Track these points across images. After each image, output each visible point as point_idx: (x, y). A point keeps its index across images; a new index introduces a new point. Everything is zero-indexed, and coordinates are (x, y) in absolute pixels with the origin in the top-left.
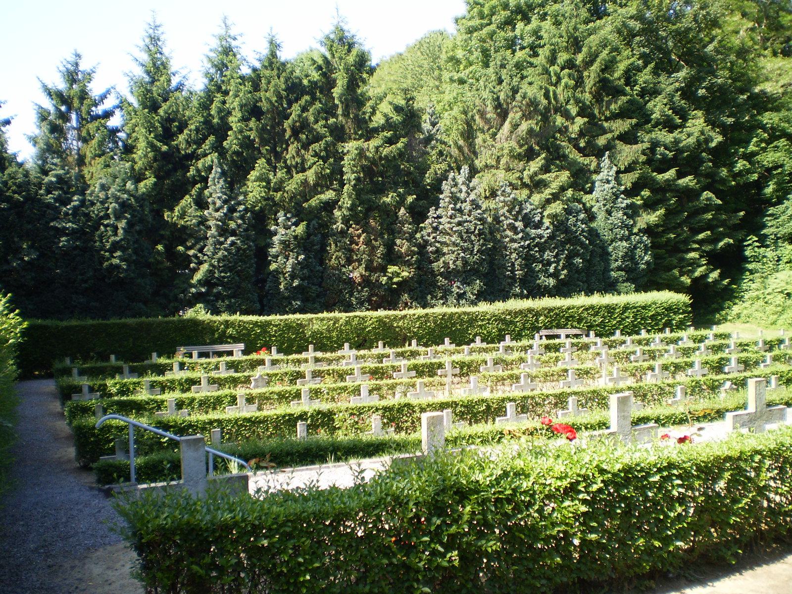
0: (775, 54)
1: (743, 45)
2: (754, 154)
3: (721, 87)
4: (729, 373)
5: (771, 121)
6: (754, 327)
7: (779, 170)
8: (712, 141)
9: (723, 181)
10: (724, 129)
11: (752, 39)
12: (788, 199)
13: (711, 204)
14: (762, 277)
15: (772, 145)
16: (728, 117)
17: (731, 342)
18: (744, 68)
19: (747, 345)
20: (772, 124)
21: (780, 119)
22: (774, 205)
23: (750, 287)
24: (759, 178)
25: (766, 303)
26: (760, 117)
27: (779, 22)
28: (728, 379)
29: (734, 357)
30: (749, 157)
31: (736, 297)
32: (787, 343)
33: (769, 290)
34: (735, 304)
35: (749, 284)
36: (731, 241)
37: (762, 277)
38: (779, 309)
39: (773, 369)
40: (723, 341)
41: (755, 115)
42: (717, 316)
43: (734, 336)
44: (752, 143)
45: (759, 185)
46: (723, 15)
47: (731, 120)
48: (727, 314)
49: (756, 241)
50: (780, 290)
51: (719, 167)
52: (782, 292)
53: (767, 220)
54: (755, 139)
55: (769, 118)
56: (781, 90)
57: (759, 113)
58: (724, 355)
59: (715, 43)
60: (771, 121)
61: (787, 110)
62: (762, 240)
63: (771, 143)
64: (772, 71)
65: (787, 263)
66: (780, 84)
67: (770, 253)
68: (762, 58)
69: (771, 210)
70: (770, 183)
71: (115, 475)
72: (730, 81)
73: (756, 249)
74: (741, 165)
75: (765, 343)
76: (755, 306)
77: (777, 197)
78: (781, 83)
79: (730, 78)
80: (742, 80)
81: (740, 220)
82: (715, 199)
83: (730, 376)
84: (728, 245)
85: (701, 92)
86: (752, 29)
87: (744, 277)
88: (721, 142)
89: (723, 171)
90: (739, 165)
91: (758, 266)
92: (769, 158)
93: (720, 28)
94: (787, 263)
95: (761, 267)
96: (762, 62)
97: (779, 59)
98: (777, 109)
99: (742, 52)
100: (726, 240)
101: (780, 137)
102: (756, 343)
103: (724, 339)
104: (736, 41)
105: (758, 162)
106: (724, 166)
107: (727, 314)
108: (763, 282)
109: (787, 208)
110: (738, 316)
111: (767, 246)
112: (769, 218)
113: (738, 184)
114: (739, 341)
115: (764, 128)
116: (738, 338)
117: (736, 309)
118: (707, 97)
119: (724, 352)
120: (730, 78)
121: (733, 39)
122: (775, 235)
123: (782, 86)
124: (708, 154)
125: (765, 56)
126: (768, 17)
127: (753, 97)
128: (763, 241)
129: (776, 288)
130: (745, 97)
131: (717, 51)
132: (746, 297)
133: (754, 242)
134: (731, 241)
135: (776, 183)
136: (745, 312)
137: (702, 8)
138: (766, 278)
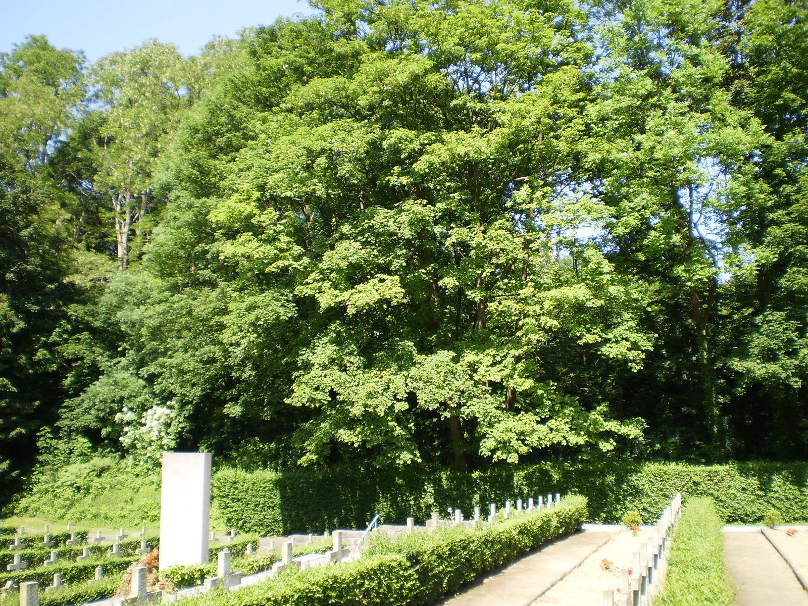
0: (88, 248)
1: (58, 235)
2: (56, 344)
3: (30, 273)
4: (11, 571)
5: (75, 314)
6: (41, 521)
7: (79, 363)
8: (14, 326)
9: (21, 368)
10: (28, 316)
11: (68, 230)
12: (85, 392)
13: (5, 392)
14: (52, 469)
15: (74, 337)
16: (33, 304)
17: (16, 538)
18: (55, 257)
19: (32, 541)
20: (77, 317)
21: (85, 313)
22: (70, 397)
23: (39, 479)
24: (58, 368)
25: (55, 496)
26: (65, 309)
27: (98, 217)
28: (10, 578)
29: (17, 554)
30: (50, 347)
31: (25, 490)
32: (72, 538)
33: (59, 483)
34: (24, 497)
35: (38, 477)
36: (23, 431)
37: (52, 469)
38: (68, 503)
39: (56, 566)
40: (7, 537)
41: (61, 306)
42: (4, 509)
43: (20, 531)
44: (54, 333)
45: (59, 376)
46: (43, 202)
47: (36, 308)
48: (14, 507)
49: (48, 432)
50: (69, 483)
51: (18, 354)
52: (72, 485)
53: (62, 412)
54: (57, 330)
55: (75, 310)
56: (89, 285)
57: (66, 305)
58: (7, 552)
59: (31, 229)
60: (75, 314)
61: (93, 304)
62: (56, 432)
63: (74, 335)
64: (83, 265)
65: (78, 455)
66: (89, 278)
67: (62, 445)
68: (75, 250)
69: (67, 402)
70: (68, 375)
71: (450, 335)
72: (39, 269)
73: (48, 440)
74: (41, 354)
75: (51, 538)
76: (44, 499)
77: (75, 389)
78: (91, 277)
79: (41, 266)
80: (55, 271)
81: (34, 409)
82: (10, 386)
83: (13, 574)
84: (20, 434)
85: (10, 276)
86: (70, 221)
87: (34, 469)
88: (22, 329)
89: (22, 358)
90: (39, 354)
91: (49, 457)
92: (70, 349)
93: (37, 213)
94: (78, 455)
95: (52, 459)
96: (75, 254)
97: (92, 254)
98: (84, 302)
99: (56, 242)
100: (18, 430)
101: (83, 330)
102: (42, 539)
103: (8, 534)
104: (51, 230)
105: (59, 352)
106: (23, 353)
107: (14, 507)
108: (53, 475)
109: (83, 401)
110: (26, 509)
111: (60, 438)
112: (63, 410)
113: (36, 374)
114: (24, 536)
115: (68, 319)
116: (23, 534)
117: (24, 502)
118: (14, 282)
119: (8, 548)
120: (41, 266)
121: (48, 227)
122: (69, 427)
123: (91, 281)
124: (9, 340)
125: (78, 249)
126: (87, 211)
127: (63, 287)
128: (56, 433)
129: (66, 482)
130: (53, 287)
131: (32, 238)
132: (35, 490)
133: (46, 433)
134: (23, 431)
135: (74, 376)
136: (33, 505)
137: (23, 192)
138: (57, 470)
